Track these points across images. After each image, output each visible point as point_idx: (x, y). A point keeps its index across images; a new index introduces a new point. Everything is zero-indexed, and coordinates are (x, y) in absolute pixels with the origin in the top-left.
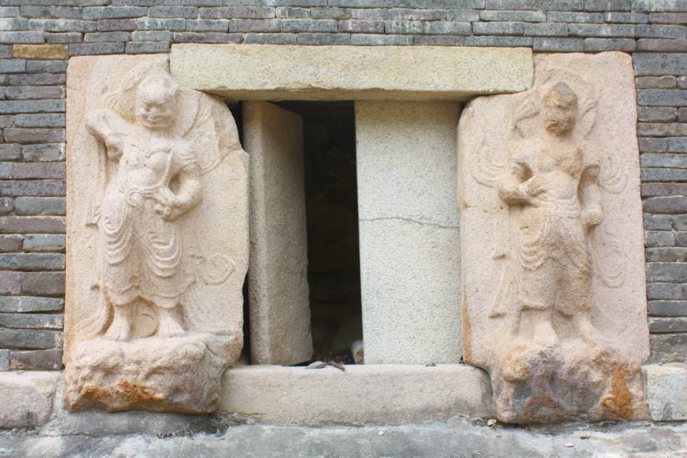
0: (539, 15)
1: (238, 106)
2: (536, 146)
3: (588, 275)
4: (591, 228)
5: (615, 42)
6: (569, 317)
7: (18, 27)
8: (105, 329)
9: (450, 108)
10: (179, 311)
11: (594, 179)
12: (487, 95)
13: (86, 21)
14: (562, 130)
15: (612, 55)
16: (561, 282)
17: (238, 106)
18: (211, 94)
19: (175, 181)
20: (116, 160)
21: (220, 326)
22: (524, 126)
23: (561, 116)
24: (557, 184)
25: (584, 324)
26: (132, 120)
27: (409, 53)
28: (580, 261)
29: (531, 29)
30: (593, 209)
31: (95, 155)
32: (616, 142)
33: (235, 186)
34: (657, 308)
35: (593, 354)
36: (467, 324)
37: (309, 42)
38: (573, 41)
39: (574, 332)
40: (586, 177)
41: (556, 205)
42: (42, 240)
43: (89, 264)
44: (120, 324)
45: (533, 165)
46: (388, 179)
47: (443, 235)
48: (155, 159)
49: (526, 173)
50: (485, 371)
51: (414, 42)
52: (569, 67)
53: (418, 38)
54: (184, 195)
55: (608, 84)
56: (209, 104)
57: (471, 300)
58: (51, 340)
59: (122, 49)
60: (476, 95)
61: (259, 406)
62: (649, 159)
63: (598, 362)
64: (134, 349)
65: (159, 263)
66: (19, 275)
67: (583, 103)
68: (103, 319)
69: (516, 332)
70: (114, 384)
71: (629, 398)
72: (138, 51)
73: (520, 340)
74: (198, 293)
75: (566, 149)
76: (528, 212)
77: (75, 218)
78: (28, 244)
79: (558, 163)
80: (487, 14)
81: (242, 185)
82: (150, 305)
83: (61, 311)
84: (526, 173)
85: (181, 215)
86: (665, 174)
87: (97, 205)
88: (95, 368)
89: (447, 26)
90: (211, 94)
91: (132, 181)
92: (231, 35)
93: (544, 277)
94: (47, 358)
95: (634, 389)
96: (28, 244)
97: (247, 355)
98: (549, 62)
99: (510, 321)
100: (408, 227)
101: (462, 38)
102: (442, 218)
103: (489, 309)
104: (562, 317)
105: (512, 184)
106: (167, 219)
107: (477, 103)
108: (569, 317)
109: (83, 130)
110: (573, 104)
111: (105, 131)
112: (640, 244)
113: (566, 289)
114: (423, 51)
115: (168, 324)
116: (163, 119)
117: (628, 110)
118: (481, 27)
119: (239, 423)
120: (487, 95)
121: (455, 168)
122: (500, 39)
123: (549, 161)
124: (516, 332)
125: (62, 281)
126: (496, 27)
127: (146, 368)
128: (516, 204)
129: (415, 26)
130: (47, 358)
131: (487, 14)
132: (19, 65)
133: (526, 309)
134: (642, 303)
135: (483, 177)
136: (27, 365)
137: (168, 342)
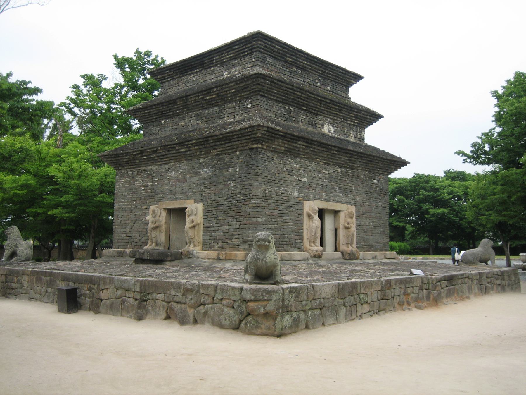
9: (336, 213)
53: (337, 202)
94: (301, 249)
101: (341, 202)
128: (347, 228)
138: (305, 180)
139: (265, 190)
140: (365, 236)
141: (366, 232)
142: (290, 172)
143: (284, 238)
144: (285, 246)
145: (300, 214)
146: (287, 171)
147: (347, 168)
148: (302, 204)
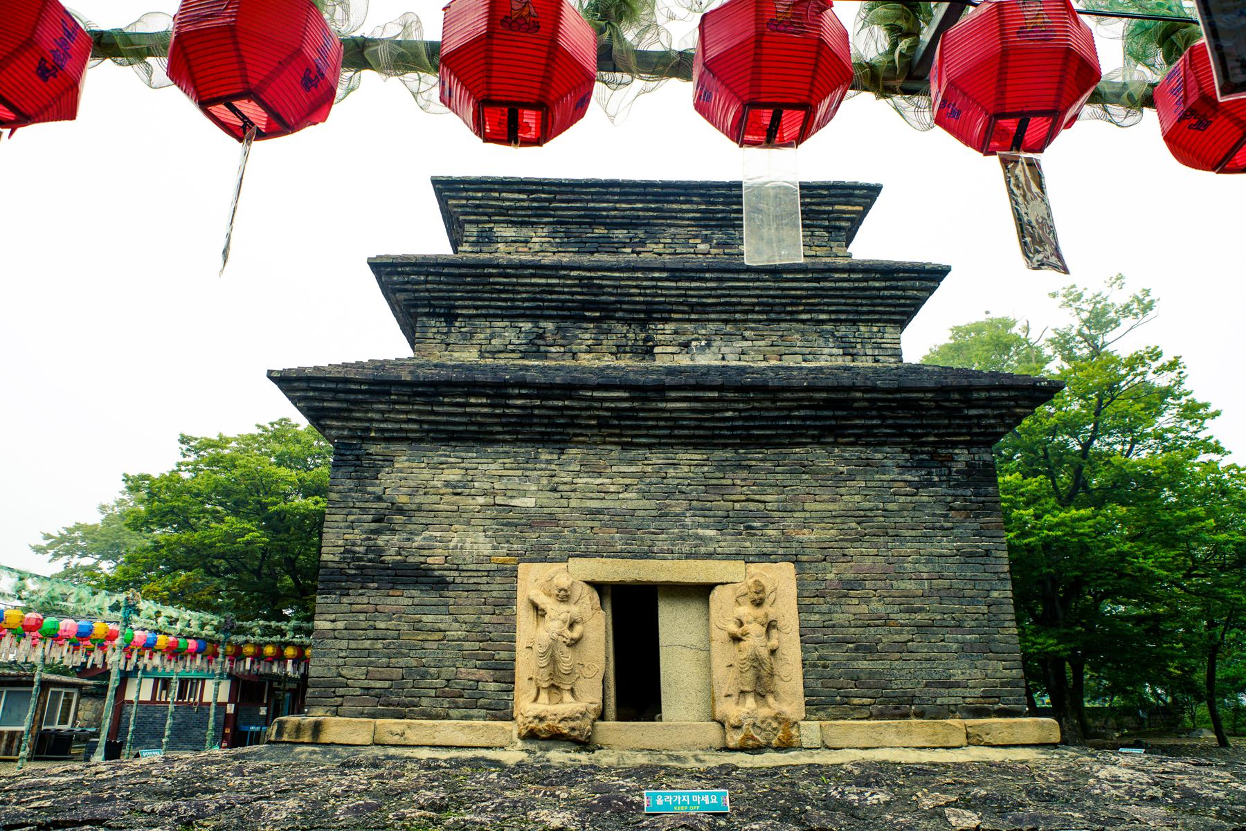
0: (748, 544)
1: (598, 587)
2: (746, 611)
3: (772, 675)
4: (773, 652)
5: (785, 558)
6: (763, 696)
7: (494, 548)
8: (536, 700)
9: (701, 592)
10: (572, 691)
11: (774, 627)
12: (722, 584)
13: (528, 545)
14: (758, 603)
15: (784, 564)
16: (758, 678)
17: (599, 587)
18: (588, 583)
19: (571, 626)
20: (543, 616)
21: (592, 699)
22: (740, 600)
23: (756, 597)
24: (755, 629)
25: (770, 699)
26: (550, 596)
27: (684, 563)
28: (767, 668)
29: (743, 551)
30: (773, 643)
31: (532, 613)
32: (786, 608)
33: (597, 627)
34: (808, 692)
35: (773, 713)
36: (714, 700)
37: (635, 557)
38: (764, 557)
39: (767, 705)
40: (770, 626)
41: (755, 641)
42: (504, 655)
43: (527, 665)
44: (544, 696)
45: (744, 620)
46: (675, 626)
47: (702, 655)
48: (563, 616)
49: (741, 624)
50: (722, 724)
51: (687, 558)
52: (760, 571)
53: (689, 556)
54: (575, 634)
55: (781, 578)
56: (587, 587)
57: (716, 688)
58: (507, 705)
59: (545, 560)
60: (717, 584)
61: (610, 741)
62: (803, 616)
63: (775, 718)
64: (552, 708)
65: (564, 667)
66: (492, 672)
67: (768, 590)
68: (534, 695)
69: (737, 703)
70: (543, 726)
71: (791, 737)
72: (553, 561)
73: (739, 707)
74: (581, 682)
75: (760, 612)
76: (742, 643)
77: (521, 643)
78: (497, 657)
79: (755, 619)
80: (723, 544)
81: (603, 628)
82: (558, 688)
83: (513, 690)
84: (741, 624)
85: (574, 643)
86: (811, 624)
87: (531, 638)
88: (535, 717)
89: (703, 550)
90: (588, 583)
91: (553, 626)
92: (598, 554)
93: (750, 676)
94: (502, 711)
95: (794, 732)
96: (497, 657)
97: (602, 717)
98: (753, 568)
99: (734, 698)
100: (684, 650)
101: (709, 556)
102: (701, 646)
103: (724, 692)
104: (760, 696)
105: (734, 628)
106: (568, 646)
107: (718, 587)
108: (763, 696)
109: (525, 600)
110: (763, 590)
111: (537, 601)
112: (800, 659)
113: (761, 682)
114: (691, 562)
115: (567, 696)
116: (564, 597)
117: (793, 591)
118: (719, 550)
119: (600, 748)
120: (722, 584)
121: (708, 620)
122: (728, 557)
123: (751, 618)
124: (737, 703)
125: (513, 676)
126: (727, 551)
127: (559, 717)
128: (736, 639)
129: (686, 549)
130: (502, 711)
131: (723, 544)
132: (494, 567)
133: (742, 692)
134: (801, 689)
135: (720, 625)
136: (495, 718)
137: (568, 706)
138: (529, 502)
139: (354, 544)
140: (863, 664)
141: (869, 650)
142: (456, 489)
143: (423, 678)
144: (425, 702)
145: (509, 600)
146: (447, 484)
147: (742, 446)
148: (514, 572)
